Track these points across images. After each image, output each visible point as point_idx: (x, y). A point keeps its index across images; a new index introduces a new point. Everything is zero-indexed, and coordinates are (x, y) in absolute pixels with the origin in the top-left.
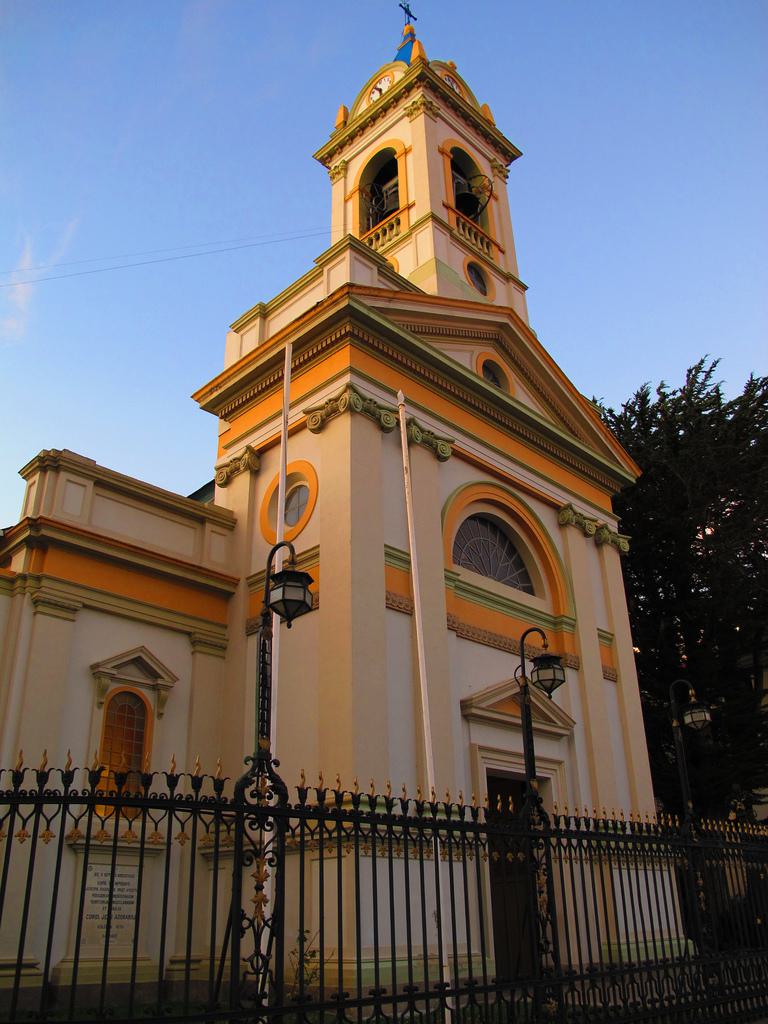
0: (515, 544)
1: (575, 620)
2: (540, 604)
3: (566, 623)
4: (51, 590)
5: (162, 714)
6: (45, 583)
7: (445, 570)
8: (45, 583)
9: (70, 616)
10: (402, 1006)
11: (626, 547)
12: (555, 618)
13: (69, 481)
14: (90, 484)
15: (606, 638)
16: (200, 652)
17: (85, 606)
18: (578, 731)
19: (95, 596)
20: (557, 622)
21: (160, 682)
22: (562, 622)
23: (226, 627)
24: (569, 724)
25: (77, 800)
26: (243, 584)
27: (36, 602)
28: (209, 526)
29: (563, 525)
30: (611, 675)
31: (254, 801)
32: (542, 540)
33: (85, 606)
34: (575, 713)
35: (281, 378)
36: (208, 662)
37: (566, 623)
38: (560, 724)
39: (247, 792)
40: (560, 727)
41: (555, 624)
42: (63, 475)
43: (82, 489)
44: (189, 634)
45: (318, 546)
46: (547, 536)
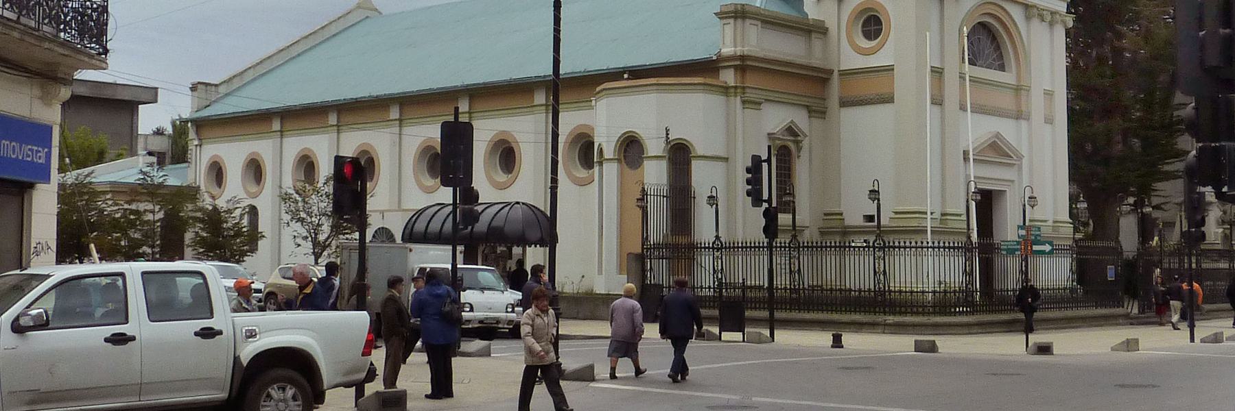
0: (1001, 45)
1: (1030, 87)
2: (1007, 77)
3: (1024, 90)
4: (751, 95)
5: (800, 156)
6: (748, 90)
7: (960, 73)
8: (748, 90)
9: (756, 107)
10: (829, 292)
11: (1071, 24)
12: (1018, 86)
13: (751, 24)
14: (759, 23)
15: (1049, 94)
16: (814, 117)
17: (767, 100)
18: (1025, 161)
19: (771, 94)
20: (1018, 89)
21: (799, 138)
22: (1021, 89)
23: (825, 100)
24: (1020, 158)
25: (913, 247)
26: (836, 74)
27: (744, 102)
28: (813, 35)
29: (1028, 18)
30: (1049, 120)
32: (1012, 30)
33: (766, 100)
34: (1024, 151)
35: (973, 150)
36: (817, 122)
37: (1024, 90)
38: (1015, 158)
40: (1015, 160)
41: (1017, 90)
42: (748, 22)
43: (755, 27)
44: (807, 107)
45: (893, 65)
46: (1015, 24)
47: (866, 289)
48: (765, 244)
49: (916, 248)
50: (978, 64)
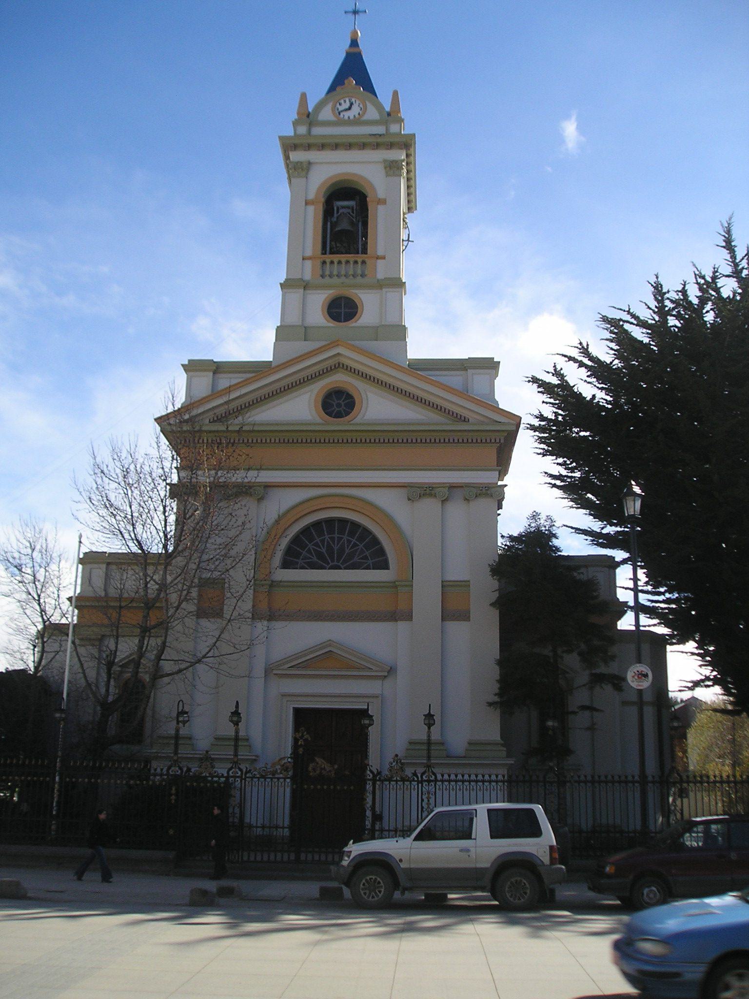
31: (426, 779)
39: (170, 771)
47: (259, 825)
48: (637, 778)
49: (497, 782)
50: (342, 567)
